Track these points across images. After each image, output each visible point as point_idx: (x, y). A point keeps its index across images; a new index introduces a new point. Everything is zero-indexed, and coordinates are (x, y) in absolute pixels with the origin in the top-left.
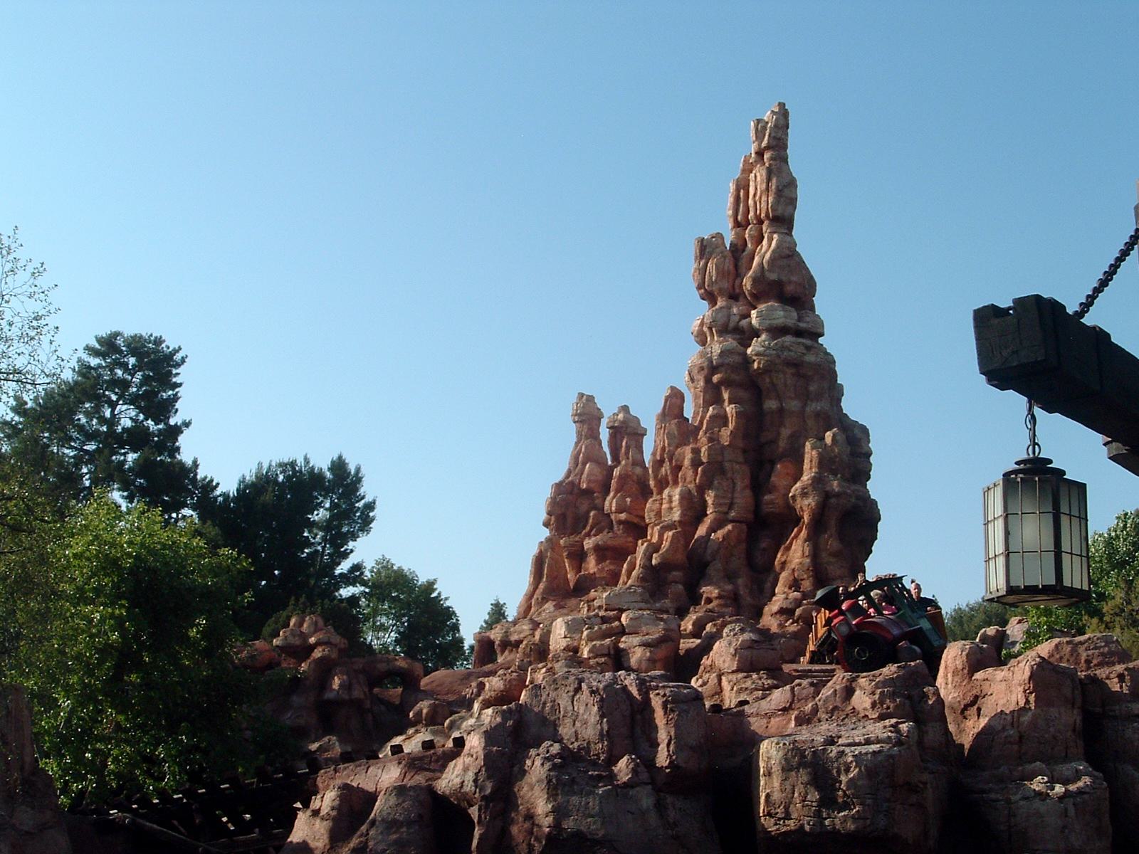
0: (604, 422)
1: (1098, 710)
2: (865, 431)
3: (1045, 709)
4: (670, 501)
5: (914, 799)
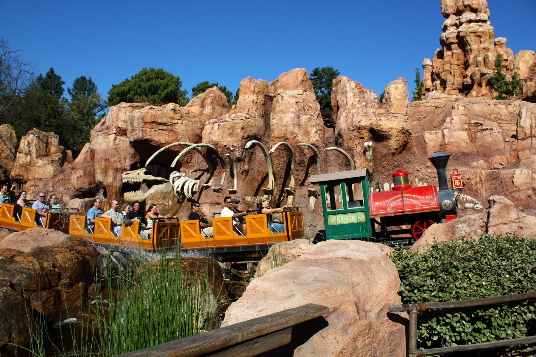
1: (272, 95)
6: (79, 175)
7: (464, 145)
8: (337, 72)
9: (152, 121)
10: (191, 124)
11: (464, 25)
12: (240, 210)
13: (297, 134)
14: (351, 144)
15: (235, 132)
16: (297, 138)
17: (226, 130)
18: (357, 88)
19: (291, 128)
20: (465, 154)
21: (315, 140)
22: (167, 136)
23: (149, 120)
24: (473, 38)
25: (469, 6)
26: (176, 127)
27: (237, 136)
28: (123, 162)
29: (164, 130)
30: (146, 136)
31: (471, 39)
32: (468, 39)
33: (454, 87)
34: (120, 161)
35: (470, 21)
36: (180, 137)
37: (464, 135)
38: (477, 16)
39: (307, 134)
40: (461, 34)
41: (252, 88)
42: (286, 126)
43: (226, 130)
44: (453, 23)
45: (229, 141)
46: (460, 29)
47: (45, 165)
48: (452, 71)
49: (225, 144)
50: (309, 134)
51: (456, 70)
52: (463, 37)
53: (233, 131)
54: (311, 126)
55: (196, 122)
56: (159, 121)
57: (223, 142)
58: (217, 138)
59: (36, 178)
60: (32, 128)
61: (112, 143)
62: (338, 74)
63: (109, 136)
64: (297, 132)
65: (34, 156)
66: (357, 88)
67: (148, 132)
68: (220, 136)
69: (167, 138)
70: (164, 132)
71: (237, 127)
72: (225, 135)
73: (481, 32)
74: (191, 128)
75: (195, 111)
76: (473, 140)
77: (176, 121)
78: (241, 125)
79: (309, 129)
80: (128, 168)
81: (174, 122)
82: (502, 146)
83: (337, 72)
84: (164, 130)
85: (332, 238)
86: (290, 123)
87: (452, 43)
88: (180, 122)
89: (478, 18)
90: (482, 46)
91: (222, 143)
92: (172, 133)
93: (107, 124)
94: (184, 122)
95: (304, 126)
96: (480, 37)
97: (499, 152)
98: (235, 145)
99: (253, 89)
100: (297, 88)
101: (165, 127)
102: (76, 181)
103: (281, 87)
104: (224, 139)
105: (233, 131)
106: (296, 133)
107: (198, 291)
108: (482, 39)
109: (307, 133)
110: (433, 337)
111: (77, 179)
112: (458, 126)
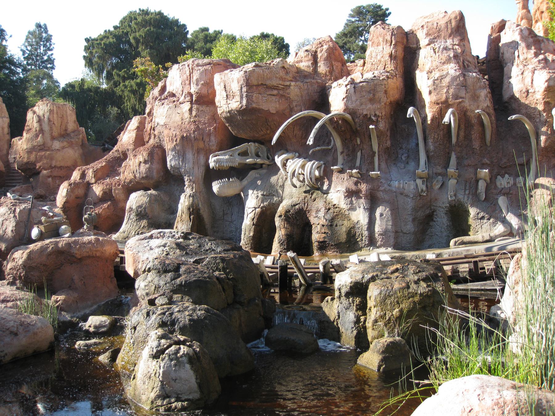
1: (415, 46)
3: (376, 48)
4: (539, 29)
8: (387, 12)
9: (260, 83)
10: (306, 87)
13: (463, 98)
15: (377, 97)
16: (463, 104)
17: (364, 94)
18: (530, 36)
21: (486, 105)
22: (277, 103)
23: (255, 83)
26: (288, 91)
27: (379, 102)
28: (207, 140)
29: (274, 95)
30: (251, 104)
34: (203, 138)
36: (294, 104)
39: (476, 98)
41: (389, 38)
43: (364, 94)
45: (370, 108)
47: (63, 148)
49: (365, 113)
50: (478, 97)
53: (374, 95)
54: (480, 87)
55: (312, 84)
56: (268, 83)
57: (363, 109)
58: (354, 105)
59: (53, 166)
61: (187, 115)
62: (390, 14)
63: (182, 106)
64: (463, 95)
65: (47, 135)
66: (530, 36)
67: (254, 98)
68: (358, 102)
69: (278, 106)
70: (274, 98)
71: (379, 90)
72: (363, 100)
74: (306, 92)
75: (306, 69)
77: (288, 83)
78: (383, 87)
79: (478, 92)
80: (214, 148)
81: (285, 84)
83: (387, 12)
84: (274, 95)
85: (374, 227)
88: (293, 84)
91: (361, 111)
92: (283, 99)
93: (169, 89)
94: (297, 83)
95: (472, 88)
98: (377, 113)
99: (389, 39)
101: (275, 92)
104: (363, 106)
105: (374, 95)
106: (461, 98)
107: (461, 290)
109: (475, 98)
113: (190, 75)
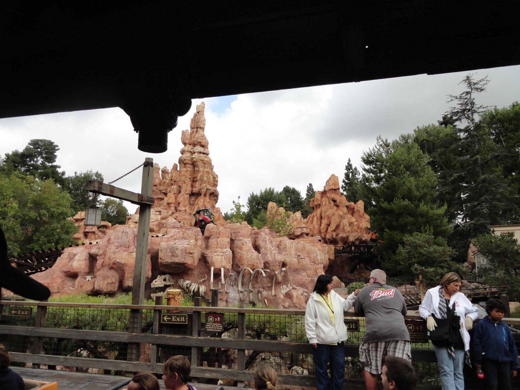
0: (160, 170)
1: (234, 238)
2: (217, 176)
5: (191, 255)
6: (110, 282)
7: (296, 265)
11: (196, 154)
12: (287, 306)
14: (274, 268)
19: (256, 261)
20: (297, 269)
24: (201, 164)
25: (200, 142)
31: (200, 164)
32: (199, 163)
33: (187, 192)
35: (200, 153)
37: (295, 260)
38: (204, 150)
40: (195, 160)
42: (254, 259)
44: (189, 151)
46: (194, 156)
48: (186, 182)
51: (189, 182)
52: (195, 162)
60: (161, 263)
73: (206, 161)
76: (299, 262)
82: (310, 266)
83: (57, 148)
86: (256, 258)
87: (188, 163)
89: (205, 152)
90: (206, 170)
96: (205, 164)
97: (310, 269)
100: (248, 237)
102: (105, 286)
103: (241, 236)
108: (206, 166)
110: (311, 357)
111: (107, 285)
112: (293, 256)
113: (134, 237)
